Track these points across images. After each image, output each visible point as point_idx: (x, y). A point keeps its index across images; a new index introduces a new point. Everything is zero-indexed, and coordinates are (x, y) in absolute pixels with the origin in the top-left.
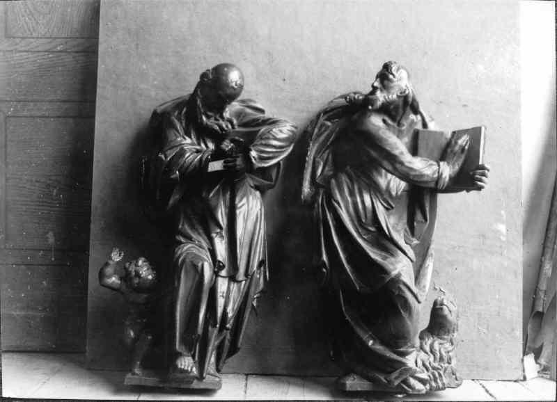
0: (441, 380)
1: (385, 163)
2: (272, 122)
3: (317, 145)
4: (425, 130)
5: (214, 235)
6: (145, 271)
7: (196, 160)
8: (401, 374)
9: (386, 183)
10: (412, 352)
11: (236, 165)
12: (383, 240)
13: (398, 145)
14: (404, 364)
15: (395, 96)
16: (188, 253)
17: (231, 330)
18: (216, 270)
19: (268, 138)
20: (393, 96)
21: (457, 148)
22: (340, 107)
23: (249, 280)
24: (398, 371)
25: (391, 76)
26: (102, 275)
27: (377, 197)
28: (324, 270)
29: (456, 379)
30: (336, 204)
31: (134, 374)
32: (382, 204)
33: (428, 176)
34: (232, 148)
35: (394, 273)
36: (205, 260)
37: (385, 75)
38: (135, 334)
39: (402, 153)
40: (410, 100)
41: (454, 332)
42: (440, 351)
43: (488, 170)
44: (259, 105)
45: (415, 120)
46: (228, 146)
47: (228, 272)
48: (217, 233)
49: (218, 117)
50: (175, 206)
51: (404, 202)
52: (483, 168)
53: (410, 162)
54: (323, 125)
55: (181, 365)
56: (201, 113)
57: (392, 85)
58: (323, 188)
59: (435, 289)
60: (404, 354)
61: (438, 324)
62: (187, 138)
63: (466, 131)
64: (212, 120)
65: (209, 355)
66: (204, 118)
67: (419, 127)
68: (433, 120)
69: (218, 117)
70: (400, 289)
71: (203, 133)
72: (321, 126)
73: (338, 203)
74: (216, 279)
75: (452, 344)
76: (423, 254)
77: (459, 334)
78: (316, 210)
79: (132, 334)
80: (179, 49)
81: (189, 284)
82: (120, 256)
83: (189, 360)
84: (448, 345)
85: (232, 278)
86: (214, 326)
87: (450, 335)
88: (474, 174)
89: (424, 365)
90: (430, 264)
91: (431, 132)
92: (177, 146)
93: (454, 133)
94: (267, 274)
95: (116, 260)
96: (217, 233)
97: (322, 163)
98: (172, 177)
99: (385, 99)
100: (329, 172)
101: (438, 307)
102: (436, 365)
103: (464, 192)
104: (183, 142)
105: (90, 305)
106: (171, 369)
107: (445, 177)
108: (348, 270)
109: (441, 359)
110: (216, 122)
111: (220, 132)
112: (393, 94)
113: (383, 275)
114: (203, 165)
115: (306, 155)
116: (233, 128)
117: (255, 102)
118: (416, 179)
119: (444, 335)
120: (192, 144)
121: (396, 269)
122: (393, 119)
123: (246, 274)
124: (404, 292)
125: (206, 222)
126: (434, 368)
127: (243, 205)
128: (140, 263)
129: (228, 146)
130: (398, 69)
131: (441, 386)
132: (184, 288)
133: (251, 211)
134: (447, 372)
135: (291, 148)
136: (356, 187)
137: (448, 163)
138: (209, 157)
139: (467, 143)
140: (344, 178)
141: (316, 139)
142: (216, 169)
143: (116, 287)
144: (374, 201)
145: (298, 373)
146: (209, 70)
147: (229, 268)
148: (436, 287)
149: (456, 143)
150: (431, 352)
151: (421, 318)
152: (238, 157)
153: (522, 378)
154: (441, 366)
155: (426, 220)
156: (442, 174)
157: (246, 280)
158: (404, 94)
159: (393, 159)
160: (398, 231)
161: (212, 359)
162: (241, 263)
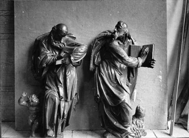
0: (140, 134)
1: (119, 60)
2: (79, 45)
3: (95, 50)
4: (133, 45)
5: (59, 86)
6: (35, 99)
7: (52, 60)
8: (126, 134)
9: (120, 65)
10: (129, 126)
11: (66, 62)
12: (119, 87)
13: (124, 53)
14: (127, 131)
15: (122, 34)
16: (50, 94)
17: (66, 119)
18: (60, 99)
19: (77, 52)
20: (122, 34)
21: (144, 53)
22: (103, 36)
23: (72, 101)
24: (124, 133)
25: (121, 27)
26: (19, 101)
27: (117, 71)
28: (98, 97)
29: (145, 133)
30: (102, 74)
31: (32, 136)
32: (118, 73)
33: (134, 64)
34: (65, 55)
35: (123, 100)
36: (56, 97)
37: (118, 26)
38: (32, 121)
39: (125, 56)
40: (128, 35)
41: (144, 117)
42: (139, 124)
43: (155, 61)
44: (74, 36)
45: (130, 42)
46: (63, 55)
47: (64, 99)
48: (60, 86)
49: (59, 42)
50: (45, 75)
51: (126, 71)
52: (153, 60)
53: (128, 60)
54: (97, 43)
55: (49, 134)
56: (53, 42)
57: (121, 30)
58: (98, 66)
59: (137, 99)
60: (126, 127)
61: (138, 115)
62: (48, 51)
63: (147, 46)
64: (57, 43)
65: (59, 126)
66: (54, 43)
67: (131, 44)
68: (136, 41)
69: (59, 42)
70: (125, 106)
71: (54, 48)
72: (96, 44)
73: (103, 74)
74: (60, 102)
75: (143, 121)
76: (133, 88)
77: (145, 117)
78: (95, 76)
79: (31, 121)
80: (44, 15)
81: (51, 105)
82: (26, 94)
83: (51, 132)
84: (142, 121)
85: (66, 101)
86: (60, 118)
87: (143, 118)
88: (151, 62)
89: (133, 129)
90: (135, 91)
91: (135, 46)
92: (44, 54)
93: (143, 46)
94: (78, 97)
95: (24, 96)
96: (60, 86)
97: (97, 57)
98: (43, 66)
99: (119, 35)
100: (99, 60)
101: (138, 109)
102: (138, 129)
103: (147, 68)
104: (47, 53)
105: (15, 108)
106: (45, 135)
107: (140, 64)
108: (107, 98)
109: (139, 127)
110: (58, 44)
111: (60, 48)
112: (122, 34)
113: (119, 101)
114: (54, 62)
115: (91, 54)
116: (65, 46)
117: (72, 35)
118: (130, 65)
119: (141, 118)
120: (50, 53)
121: (123, 98)
122: (122, 42)
123: (71, 99)
124: (126, 106)
125: (56, 81)
126: (137, 130)
127: (69, 75)
128: (33, 96)
129: (63, 55)
130: (123, 24)
131: (139, 136)
132: (49, 107)
133: (73, 75)
134: (142, 131)
135: (86, 54)
136: (109, 67)
137: (141, 58)
138: (56, 58)
139: (148, 51)
140: (105, 64)
141: (94, 48)
142: (59, 64)
143: (25, 105)
144: (115, 71)
145: (91, 130)
146: (55, 26)
147: (65, 98)
148: (138, 99)
149: (144, 50)
150: (136, 124)
151: (133, 112)
152: (66, 59)
153: (167, 128)
154: (139, 129)
155: (134, 77)
156: (139, 63)
157: (71, 101)
158: (126, 33)
159: (122, 59)
160: (124, 82)
161: (60, 128)
162: (69, 92)
